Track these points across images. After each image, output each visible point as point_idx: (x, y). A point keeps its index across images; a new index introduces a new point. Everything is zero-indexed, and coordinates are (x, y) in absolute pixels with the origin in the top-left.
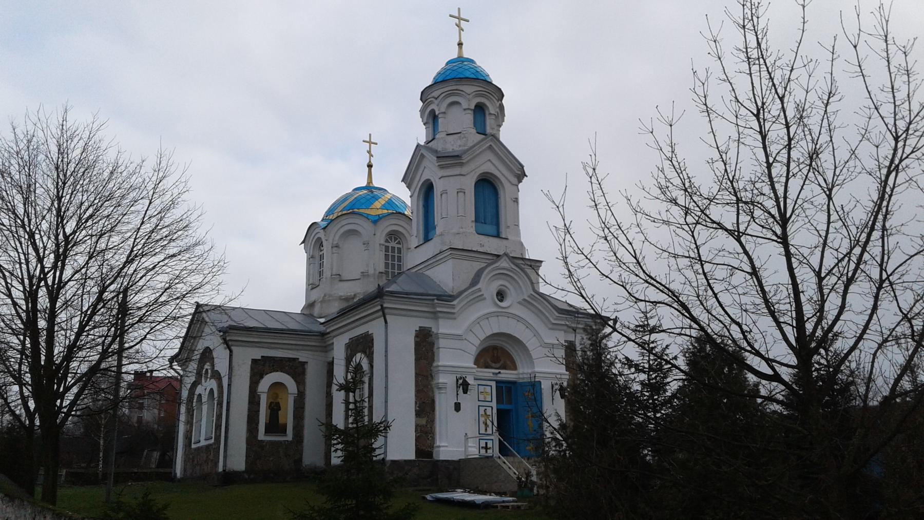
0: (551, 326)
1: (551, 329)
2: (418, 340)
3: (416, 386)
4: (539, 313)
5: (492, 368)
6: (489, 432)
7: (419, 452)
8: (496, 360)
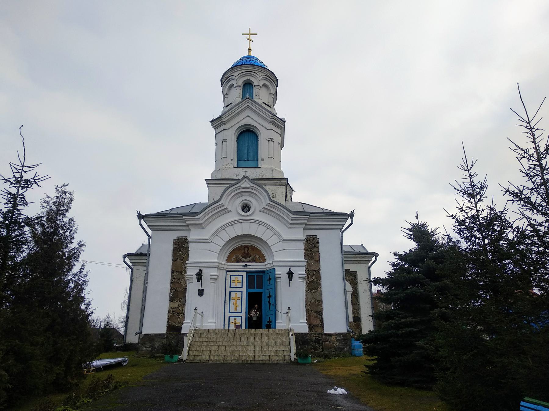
0: (289, 225)
1: (289, 228)
3: (172, 279)
4: (278, 217)
5: (242, 262)
6: (239, 310)
7: (170, 327)
8: (247, 255)
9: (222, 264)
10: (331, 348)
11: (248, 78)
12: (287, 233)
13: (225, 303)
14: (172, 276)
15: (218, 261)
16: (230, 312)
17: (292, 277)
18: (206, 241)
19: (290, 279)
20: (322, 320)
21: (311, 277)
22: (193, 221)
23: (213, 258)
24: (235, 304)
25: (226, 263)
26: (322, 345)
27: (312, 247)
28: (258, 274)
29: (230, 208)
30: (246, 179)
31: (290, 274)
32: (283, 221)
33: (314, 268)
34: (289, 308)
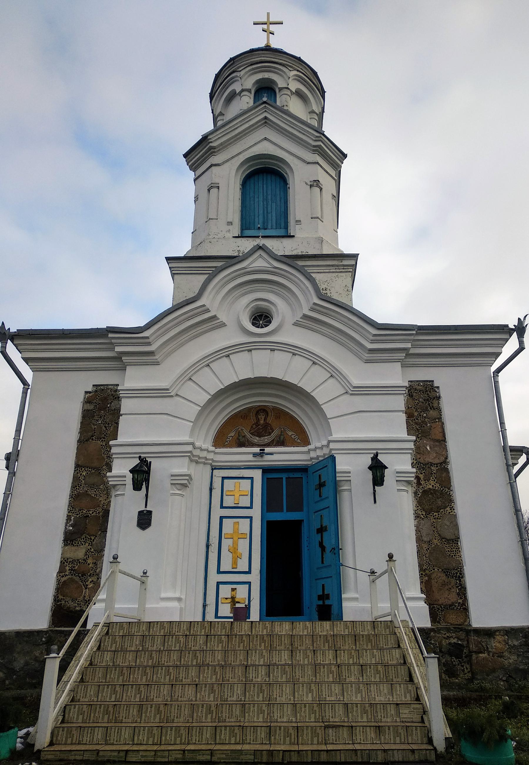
0: (367, 356)
1: (368, 361)
2: (90, 407)
6: (243, 565)
8: (262, 430)
9: (201, 449)
10: (494, 671)
11: (266, 75)
12: (359, 374)
13: (208, 546)
14: (76, 479)
15: (191, 440)
16: (219, 572)
17: (383, 476)
18: (162, 393)
19: (378, 480)
20: (462, 591)
21: (427, 479)
22: (133, 344)
23: (179, 433)
24: (234, 550)
25: (213, 449)
26: (470, 662)
27: (423, 408)
28: (291, 475)
29: (223, 317)
30: (260, 252)
31: (377, 469)
32: (352, 345)
33: (431, 458)
34: (391, 556)
